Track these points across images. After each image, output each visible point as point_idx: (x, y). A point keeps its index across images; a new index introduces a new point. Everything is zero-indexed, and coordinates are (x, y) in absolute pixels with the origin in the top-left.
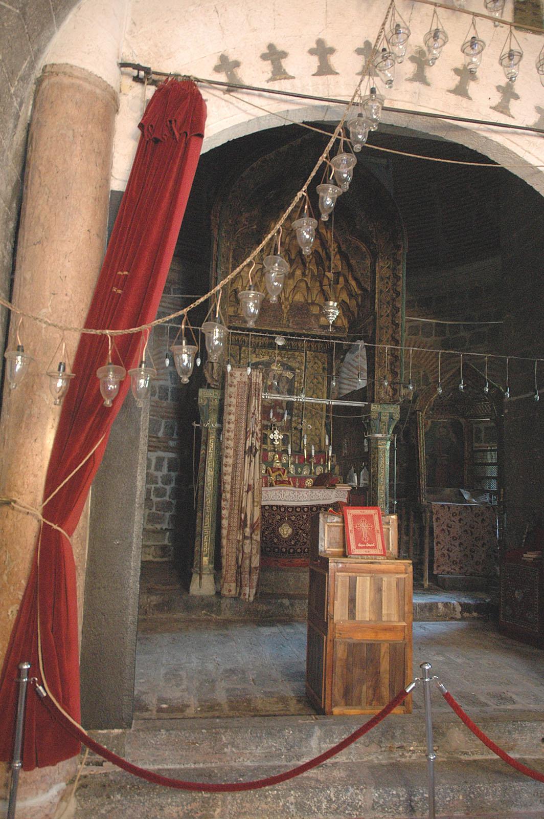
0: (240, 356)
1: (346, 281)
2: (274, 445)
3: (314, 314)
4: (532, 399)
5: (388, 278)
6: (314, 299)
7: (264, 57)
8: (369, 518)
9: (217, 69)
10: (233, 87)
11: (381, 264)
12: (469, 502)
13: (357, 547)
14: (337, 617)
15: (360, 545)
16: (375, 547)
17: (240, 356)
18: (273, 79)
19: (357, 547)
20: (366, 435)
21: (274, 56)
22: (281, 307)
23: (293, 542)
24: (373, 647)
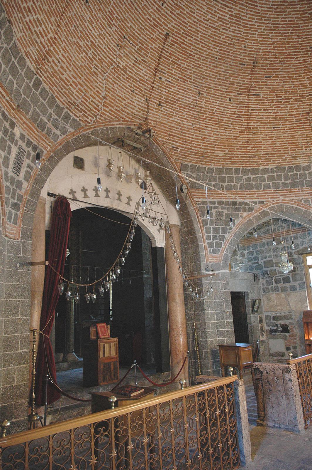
7: (82, 190)
8: (104, 326)
9: (70, 193)
10: (74, 199)
12: (93, 319)
14: (101, 357)
18: (84, 197)
21: (84, 190)
24: (109, 364)
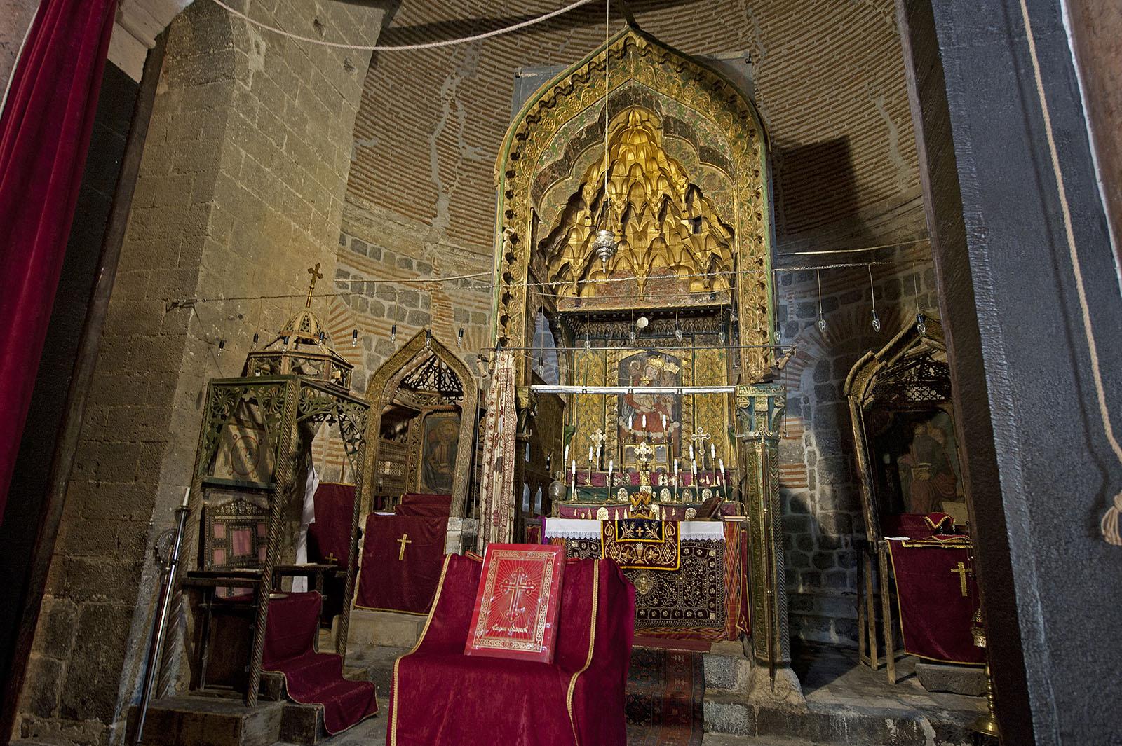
4: (985, 673)
5: (749, 201)
6: (677, 261)
23: (656, 601)
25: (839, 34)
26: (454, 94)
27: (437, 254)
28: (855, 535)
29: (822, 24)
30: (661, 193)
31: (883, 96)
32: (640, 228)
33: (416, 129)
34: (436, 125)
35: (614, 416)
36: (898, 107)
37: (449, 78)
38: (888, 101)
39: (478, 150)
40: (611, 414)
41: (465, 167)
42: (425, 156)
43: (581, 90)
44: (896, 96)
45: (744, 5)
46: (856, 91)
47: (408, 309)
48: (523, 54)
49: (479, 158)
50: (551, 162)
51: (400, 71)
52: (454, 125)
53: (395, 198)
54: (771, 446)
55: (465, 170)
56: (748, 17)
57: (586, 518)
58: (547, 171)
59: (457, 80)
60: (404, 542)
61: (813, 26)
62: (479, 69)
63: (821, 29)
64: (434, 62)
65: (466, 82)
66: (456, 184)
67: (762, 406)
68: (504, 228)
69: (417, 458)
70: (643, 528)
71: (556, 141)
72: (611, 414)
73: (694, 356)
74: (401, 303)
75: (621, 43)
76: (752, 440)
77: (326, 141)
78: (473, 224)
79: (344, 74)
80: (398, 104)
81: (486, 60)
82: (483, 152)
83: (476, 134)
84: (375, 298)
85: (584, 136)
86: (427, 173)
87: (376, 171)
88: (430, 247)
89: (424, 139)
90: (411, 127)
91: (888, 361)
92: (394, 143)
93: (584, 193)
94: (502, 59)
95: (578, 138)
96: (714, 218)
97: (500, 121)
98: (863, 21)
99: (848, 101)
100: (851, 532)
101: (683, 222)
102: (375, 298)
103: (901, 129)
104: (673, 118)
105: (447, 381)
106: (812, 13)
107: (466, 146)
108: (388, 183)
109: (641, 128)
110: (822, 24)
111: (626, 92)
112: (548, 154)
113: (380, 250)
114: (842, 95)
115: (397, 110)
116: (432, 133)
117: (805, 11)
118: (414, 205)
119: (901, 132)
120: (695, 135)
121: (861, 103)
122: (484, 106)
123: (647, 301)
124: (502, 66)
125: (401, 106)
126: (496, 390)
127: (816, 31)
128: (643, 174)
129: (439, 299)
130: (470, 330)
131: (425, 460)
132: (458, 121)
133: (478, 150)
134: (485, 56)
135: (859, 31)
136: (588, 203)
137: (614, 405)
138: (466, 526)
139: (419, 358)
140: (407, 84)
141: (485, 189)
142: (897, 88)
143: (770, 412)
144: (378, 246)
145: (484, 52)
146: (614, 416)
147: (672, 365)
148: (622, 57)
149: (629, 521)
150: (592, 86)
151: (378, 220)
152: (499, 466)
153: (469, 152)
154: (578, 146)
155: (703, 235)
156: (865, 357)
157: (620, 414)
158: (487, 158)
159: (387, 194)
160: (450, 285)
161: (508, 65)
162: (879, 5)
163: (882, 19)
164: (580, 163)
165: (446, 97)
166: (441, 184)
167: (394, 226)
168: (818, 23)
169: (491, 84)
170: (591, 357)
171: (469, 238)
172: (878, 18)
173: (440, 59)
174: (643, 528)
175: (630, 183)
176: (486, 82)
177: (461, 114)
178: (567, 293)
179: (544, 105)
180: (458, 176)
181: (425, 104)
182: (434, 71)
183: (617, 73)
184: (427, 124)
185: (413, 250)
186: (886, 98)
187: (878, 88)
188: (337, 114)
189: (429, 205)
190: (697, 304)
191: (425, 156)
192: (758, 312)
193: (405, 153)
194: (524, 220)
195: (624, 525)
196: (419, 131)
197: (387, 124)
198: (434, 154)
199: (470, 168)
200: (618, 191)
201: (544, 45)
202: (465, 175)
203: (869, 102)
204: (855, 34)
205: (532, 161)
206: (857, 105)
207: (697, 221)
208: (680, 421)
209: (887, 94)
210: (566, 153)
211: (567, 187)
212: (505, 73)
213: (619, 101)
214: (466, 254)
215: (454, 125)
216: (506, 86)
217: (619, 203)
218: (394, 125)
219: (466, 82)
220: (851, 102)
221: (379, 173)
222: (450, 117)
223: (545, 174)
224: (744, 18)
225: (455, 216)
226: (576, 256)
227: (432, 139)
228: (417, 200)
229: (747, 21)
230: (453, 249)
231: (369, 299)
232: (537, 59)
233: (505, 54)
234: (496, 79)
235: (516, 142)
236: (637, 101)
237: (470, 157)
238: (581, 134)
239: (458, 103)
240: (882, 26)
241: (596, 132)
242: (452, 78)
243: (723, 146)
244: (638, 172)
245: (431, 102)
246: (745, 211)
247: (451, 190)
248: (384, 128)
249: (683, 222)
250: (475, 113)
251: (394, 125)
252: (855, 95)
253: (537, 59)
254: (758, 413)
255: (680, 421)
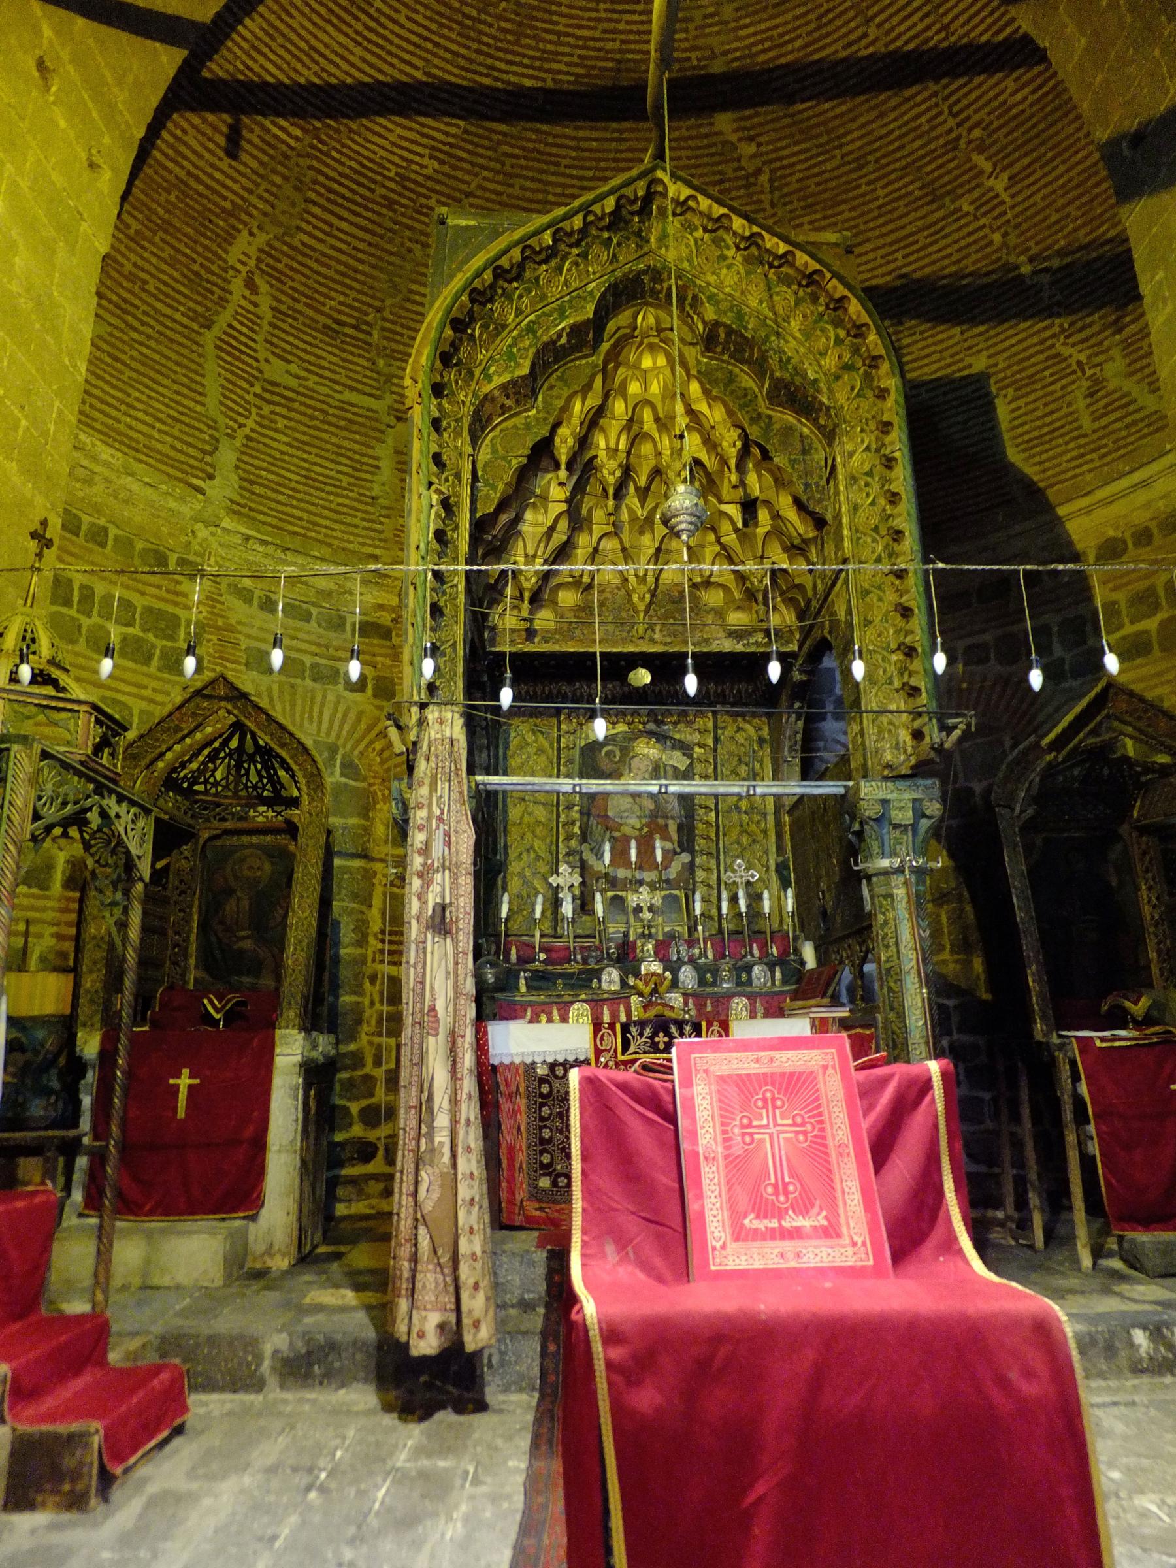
0: (559, 729)
1: (776, 516)
2: (642, 920)
3: (713, 609)
5: (870, 474)
11: (849, 447)
13: (740, 1234)
15: (750, 1222)
16: (830, 1232)
17: (559, 729)
19: (740, 1234)
20: (856, 864)
22: (630, 600)
25: (918, 251)
26: (253, 263)
27: (215, 546)
28: (955, 1037)
29: (892, 231)
30: (687, 457)
31: (985, 353)
32: (641, 513)
33: (178, 316)
34: (217, 313)
35: (573, 843)
36: (1009, 372)
37: (245, 233)
38: (992, 361)
39: (293, 368)
40: (569, 838)
41: (267, 395)
42: (194, 366)
43: (565, 258)
44: (1005, 355)
45: (767, 185)
46: (942, 341)
47: (160, 643)
48: (384, 211)
49: (293, 383)
50: (505, 378)
51: (154, 206)
52: (252, 320)
53: (136, 435)
54: (917, 883)
55: (269, 402)
56: (773, 205)
57: (550, 1021)
58: (496, 393)
59: (261, 239)
60: (184, 1081)
61: (877, 233)
62: (304, 225)
63: (889, 240)
64: (218, 199)
65: (276, 244)
66: (250, 424)
67: (904, 816)
68: (430, 484)
69: (188, 921)
70: (668, 1034)
71: (514, 344)
72: (569, 838)
73: (717, 740)
74: (145, 630)
75: (641, 189)
76: (886, 873)
77: (50, 296)
78: (281, 498)
79: (87, 173)
80: (146, 266)
81: (317, 210)
82: (303, 374)
83: (291, 339)
84: (95, 619)
85: (563, 340)
86: (198, 398)
87: (101, 383)
88: (203, 532)
89: (194, 335)
90: (168, 311)
91: (1059, 752)
92: (135, 335)
93: (557, 441)
94: (345, 214)
95: (554, 342)
96: (785, 503)
97: (336, 321)
98: (957, 236)
99: (928, 356)
100: (950, 1034)
101: (724, 507)
102: (95, 619)
103: (1013, 405)
104: (725, 325)
105: (254, 779)
106: (876, 213)
107: (272, 358)
108: (123, 407)
109: (656, 340)
110: (892, 231)
111: (640, 273)
112: (499, 365)
113: (105, 530)
114: (920, 345)
115: (142, 275)
116: (209, 328)
117: (866, 208)
118: (172, 453)
119: (1013, 411)
120: (764, 358)
121: (949, 361)
122: (307, 291)
123: (652, 640)
124: (344, 225)
125: (154, 271)
126: (427, 781)
127: (881, 242)
128: (657, 420)
129: (219, 629)
130: (275, 687)
131: (204, 926)
132: (258, 311)
133: (293, 368)
134: (315, 204)
135: (949, 250)
136: (563, 459)
137: (573, 823)
138: (308, 1046)
139: (209, 730)
140: (166, 232)
141: (305, 438)
142: (1007, 343)
143: (914, 827)
144: (102, 522)
145: (313, 196)
146: (573, 843)
147: (677, 754)
148: (639, 213)
149: (642, 1024)
150: (584, 255)
151: (107, 473)
152: (440, 923)
153: (276, 370)
154: (550, 357)
155: (761, 531)
156: (1026, 743)
157: (584, 838)
158: (310, 384)
159: (122, 427)
160: (238, 604)
161: (356, 226)
162: (984, 214)
163: (986, 236)
164: (551, 387)
165: (239, 266)
166: (222, 421)
167: (136, 487)
168: (884, 230)
169: (324, 254)
170: (530, 738)
171: (274, 522)
172: (981, 233)
173: (231, 196)
174: (668, 1034)
175: (633, 433)
176: (314, 249)
177: (265, 303)
178: (507, 619)
179: (500, 273)
180: (254, 410)
181: (197, 274)
182: (217, 216)
183: (628, 239)
184: (199, 308)
185: (170, 535)
186: (989, 357)
187: (975, 341)
188: (72, 249)
189: (200, 456)
190: (739, 648)
191: (194, 366)
192: (894, 657)
193: (157, 357)
194: (458, 476)
195: (634, 1030)
196: (185, 320)
197: (124, 300)
198: (211, 366)
199: (276, 398)
200: (612, 444)
201: (423, 201)
202: (267, 409)
203: (962, 360)
204: (942, 254)
205: (471, 373)
206: (943, 363)
207: (749, 507)
208: (692, 853)
209: (992, 351)
210: (533, 366)
211: (528, 426)
212: (349, 239)
213: (626, 287)
214: (270, 549)
215: (252, 320)
216: (351, 262)
217: (612, 464)
218: (137, 302)
219: (276, 244)
220: (934, 357)
221: (106, 387)
222: (243, 303)
223: (493, 399)
224: (767, 205)
225: (248, 482)
226: (531, 552)
227: (209, 338)
228: (178, 445)
229: (770, 211)
230: (247, 538)
231: (85, 622)
232: (409, 222)
233: (349, 205)
234: (333, 247)
235: (449, 332)
236: (655, 293)
237: (278, 380)
238: (559, 336)
239: (258, 280)
240: (987, 246)
241: (586, 336)
242: (251, 234)
243: (816, 381)
244: (647, 415)
245: (210, 271)
246: (861, 490)
247: (240, 433)
248: (117, 306)
249: (724, 507)
250: (291, 302)
251: (137, 302)
252: (939, 347)
253: (409, 222)
254: (896, 826)
255: (692, 853)
